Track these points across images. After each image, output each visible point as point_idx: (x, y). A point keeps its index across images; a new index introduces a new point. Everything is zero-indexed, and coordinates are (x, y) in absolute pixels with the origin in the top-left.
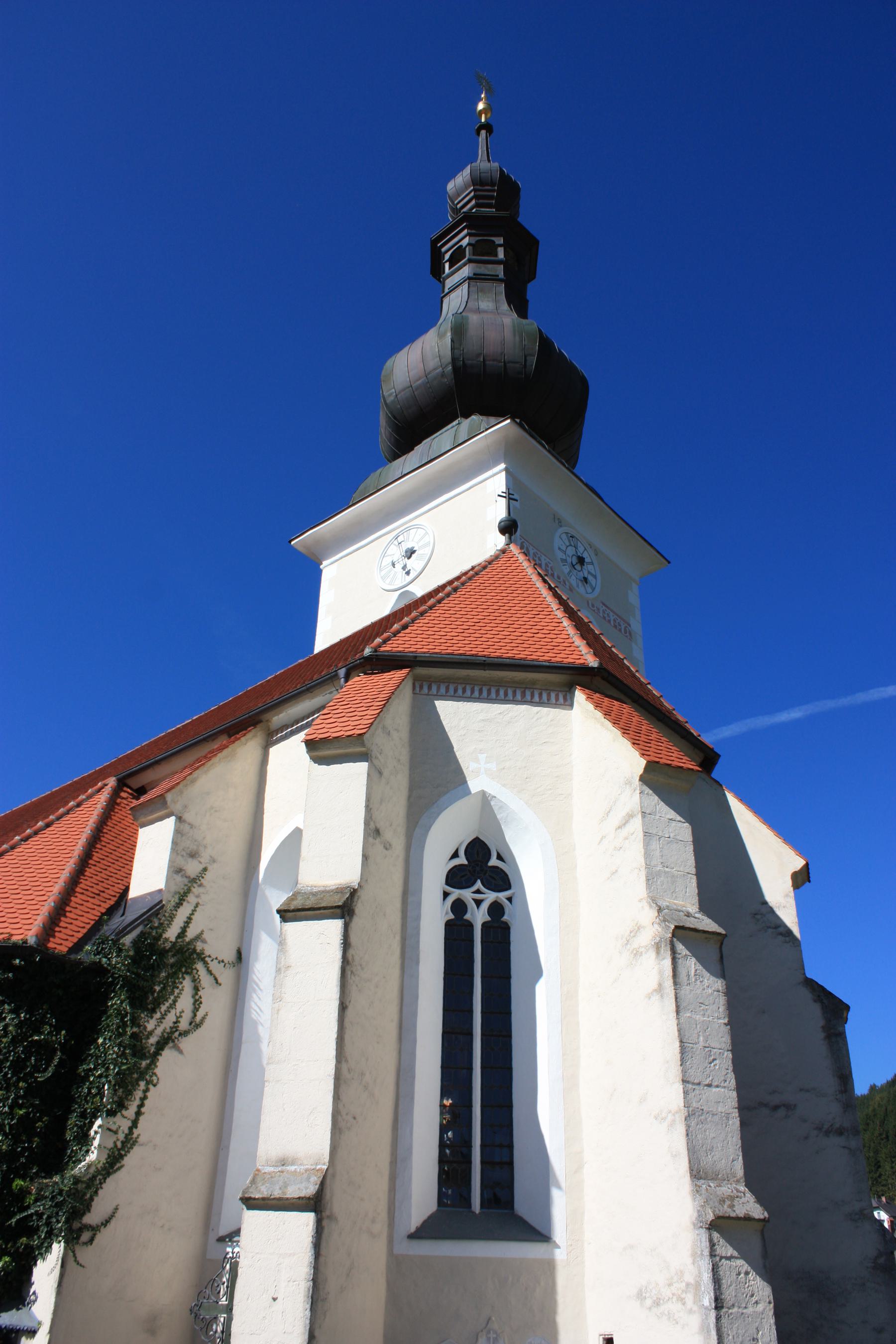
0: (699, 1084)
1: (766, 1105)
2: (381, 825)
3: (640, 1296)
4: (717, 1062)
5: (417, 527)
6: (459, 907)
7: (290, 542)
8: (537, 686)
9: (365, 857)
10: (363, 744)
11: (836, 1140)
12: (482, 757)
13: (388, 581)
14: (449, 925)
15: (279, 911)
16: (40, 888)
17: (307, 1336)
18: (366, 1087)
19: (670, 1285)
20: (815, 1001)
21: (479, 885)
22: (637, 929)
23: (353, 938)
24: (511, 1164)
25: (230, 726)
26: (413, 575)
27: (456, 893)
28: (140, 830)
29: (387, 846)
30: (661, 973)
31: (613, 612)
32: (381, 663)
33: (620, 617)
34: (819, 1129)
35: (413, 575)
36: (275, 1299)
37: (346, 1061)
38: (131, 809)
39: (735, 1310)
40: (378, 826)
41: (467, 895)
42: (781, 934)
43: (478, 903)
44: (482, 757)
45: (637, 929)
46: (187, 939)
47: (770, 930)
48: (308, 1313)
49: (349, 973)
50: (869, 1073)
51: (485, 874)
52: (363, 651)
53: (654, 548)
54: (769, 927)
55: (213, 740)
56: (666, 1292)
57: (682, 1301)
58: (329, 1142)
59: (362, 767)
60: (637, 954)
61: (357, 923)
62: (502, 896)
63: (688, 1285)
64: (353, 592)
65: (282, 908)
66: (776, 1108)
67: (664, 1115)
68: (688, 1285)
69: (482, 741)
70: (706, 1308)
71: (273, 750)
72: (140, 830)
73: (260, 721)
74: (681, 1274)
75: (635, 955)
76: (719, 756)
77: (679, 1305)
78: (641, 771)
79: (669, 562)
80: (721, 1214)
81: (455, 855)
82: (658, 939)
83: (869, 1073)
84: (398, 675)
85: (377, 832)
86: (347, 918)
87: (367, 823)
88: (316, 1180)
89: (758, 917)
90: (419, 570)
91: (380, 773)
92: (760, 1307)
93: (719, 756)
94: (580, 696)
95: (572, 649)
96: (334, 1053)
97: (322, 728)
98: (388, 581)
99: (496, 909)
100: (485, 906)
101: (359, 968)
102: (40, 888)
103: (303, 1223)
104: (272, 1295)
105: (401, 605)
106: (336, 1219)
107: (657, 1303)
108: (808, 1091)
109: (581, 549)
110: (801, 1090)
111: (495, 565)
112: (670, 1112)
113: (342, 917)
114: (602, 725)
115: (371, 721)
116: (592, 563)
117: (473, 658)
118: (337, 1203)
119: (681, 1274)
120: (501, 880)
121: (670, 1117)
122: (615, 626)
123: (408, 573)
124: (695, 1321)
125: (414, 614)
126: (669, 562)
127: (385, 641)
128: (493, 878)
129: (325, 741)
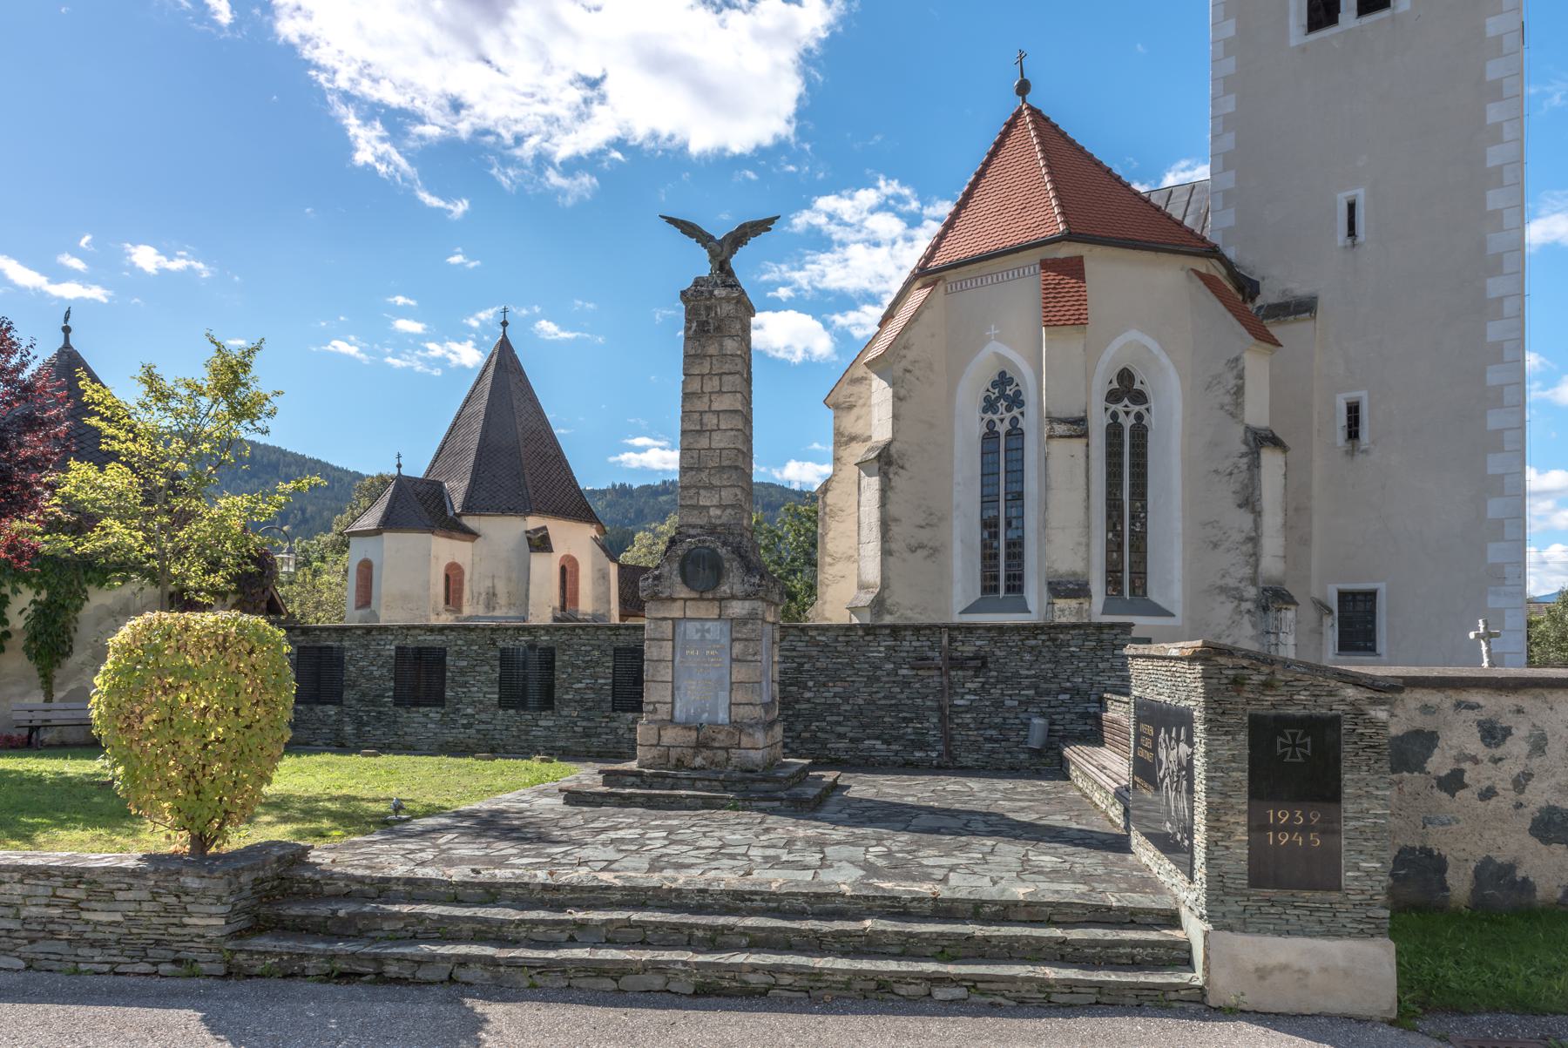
6: (1114, 416)
14: (985, 438)
21: (1126, 401)
24: (1022, 471)
27: (1113, 407)
28: (719, 237)
41: (1119, 408)
43: (1127, 413)
46: (862, 873)
50: (1541, 582)
62: (1141, 408)
71: (61, 343)
72: (719, 237)
83: (1541, 582)
99: (1014, 420)
100: (1132, 416)
120: (1140, 398)
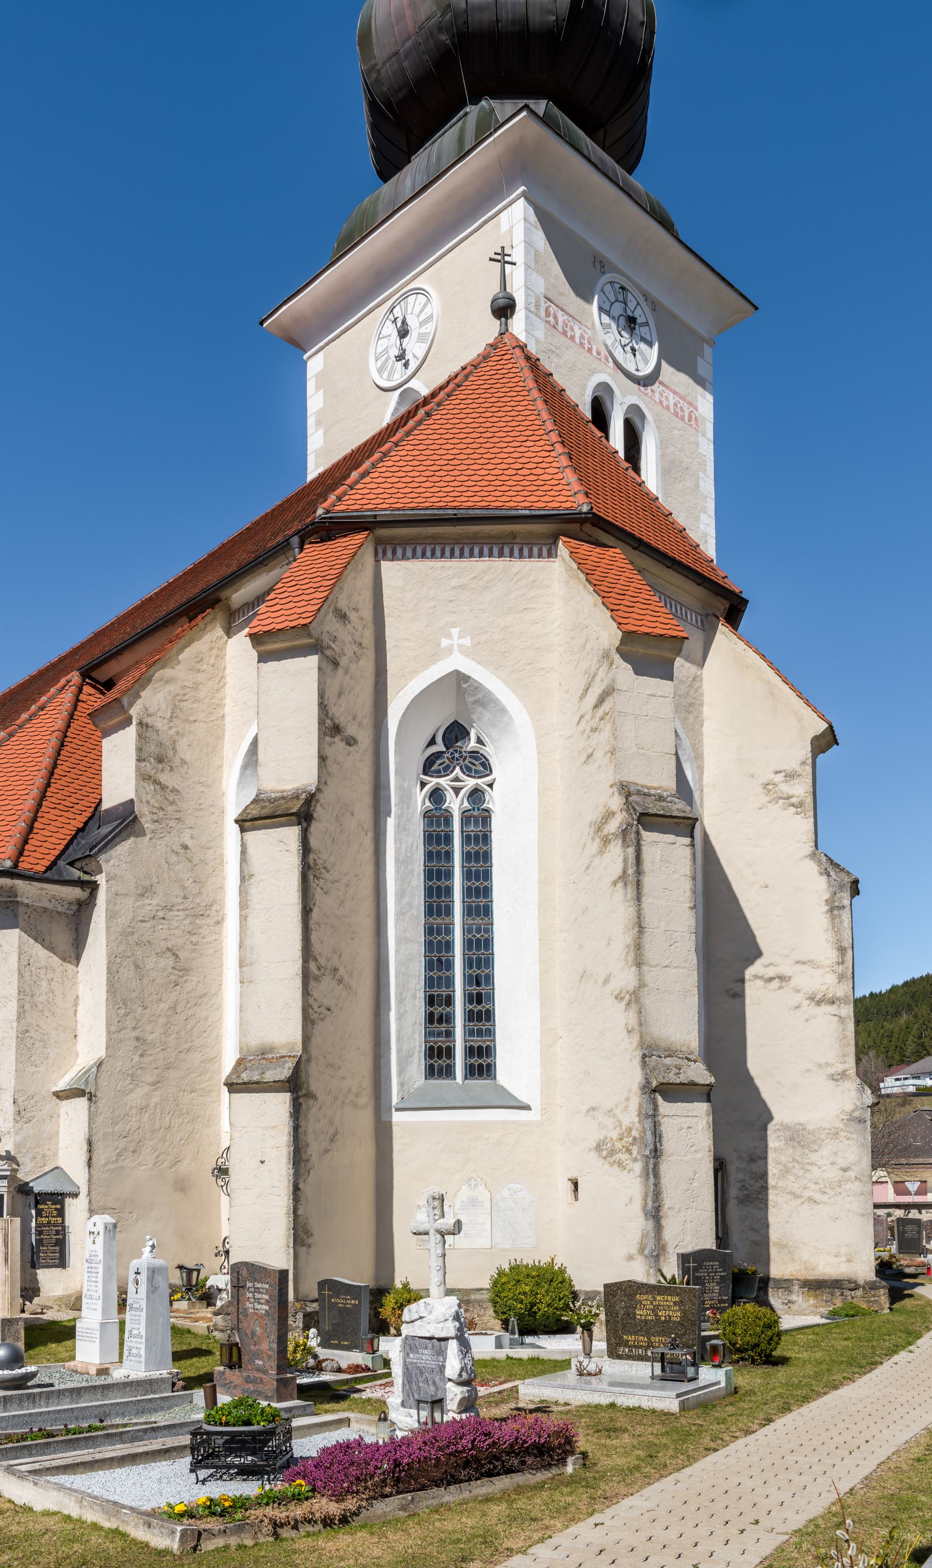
0: (657, 966)
1: (761, 978)
2: (342, 720)
3: (598, 1148)
4: (678, 944)
5: (418, 291)
6: (437, 795)
7: (261, 323)
8: (517, 540)
9: (322, 759)
10: (310, 635)
11: (826, 1008)
12: (455, 632)
13: (385, 375)
15: (236, 821)
16: (10, 807)
17: (291, 1188)
18: (340, 981)
19: (621, 1139)
20: (821, 874)
22: (610, 815)
23: (313, 842)
25: (186, 609)
26: (413, 366)
27: (433, 782)
29: (351, 742)
30: (625, 860)
31: (675, 393)
32: (331, 530)
33: (684, 399)
34: (811, 998)
35: (413, 366)
36: (262, 1162)
37: (316, 960)
38: (89, 715)
39: (675, 1157)
40: (337, 722)
42: (793, 805)
43: (457, 791)
44: (455, 632)
45: (610, 815)
47: (781, 801)
48: (291, 1172)
49: (311, 877)
51: (464, 760)
52: (315, 512)
53: (736, 290)
54: (781, 798)
55: (173, 624)
56: (619, 1145)
57: (629, 1151)
58: (301, 1033)
59: (312, 661)
60: (606, 841)
61: (315, 829)
63: (635, 1139)
64: (347, 393)
65: (240, 818)
66: (771, 979)
67: (623, 995)
68: (635, 1139)
69: (454, 612)
70: (647, 1157)
73: (218, 601)
74: (630, 1130)
75: (605, 842)
76: (746, 602)
77: (627, 1155)
78: (617, 643)
79: (757, 308)
80: (664, 1081)
81: (432, 742)
82: (625, 826)
84: (360, 537)
85: (336, 729)
86: (305, 825)
87: (321, 723)
88: (290, 1064)
89: (770, 787)
90: (421, 356)
91: (336, 664)
92: (699, 1155)
93: (746, 602)
94: (562, 549)
95: (560, 487)
96: (300, 954)
97: (267, 617)
98: (385, 375)
101: (323, 871)
102: (10, 807)
103: (281, 1102)
104: (260, 1158)
105: (403, 410)
106: (315, 1097)
107: (612, 1153)
108: (804, 963)
109: (632, 304)
110: (797, 963)
111: (485, 368)
112: (628, 992)
113: (299, 824)
114: (585, 587)
115: (317, 607)
116: (646, 324)
117: (441, 512)
118: (316, 1081)
119: (630, 1130)
121: (628, 997)
122: (676, 414)
123: (406, 365)
124: (638, 1167)
125: (411, 423)
126: (757, 308)
127: (339, 499)
128: (474, 765)
129: (270, 634)
